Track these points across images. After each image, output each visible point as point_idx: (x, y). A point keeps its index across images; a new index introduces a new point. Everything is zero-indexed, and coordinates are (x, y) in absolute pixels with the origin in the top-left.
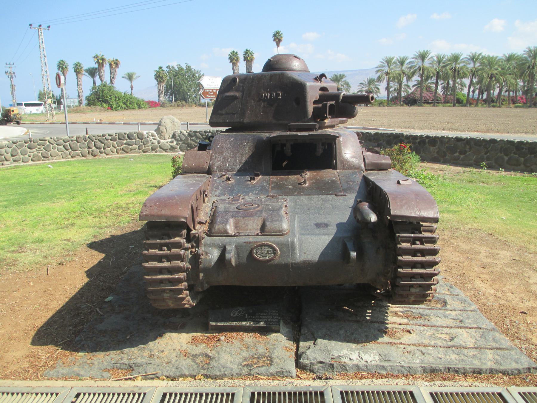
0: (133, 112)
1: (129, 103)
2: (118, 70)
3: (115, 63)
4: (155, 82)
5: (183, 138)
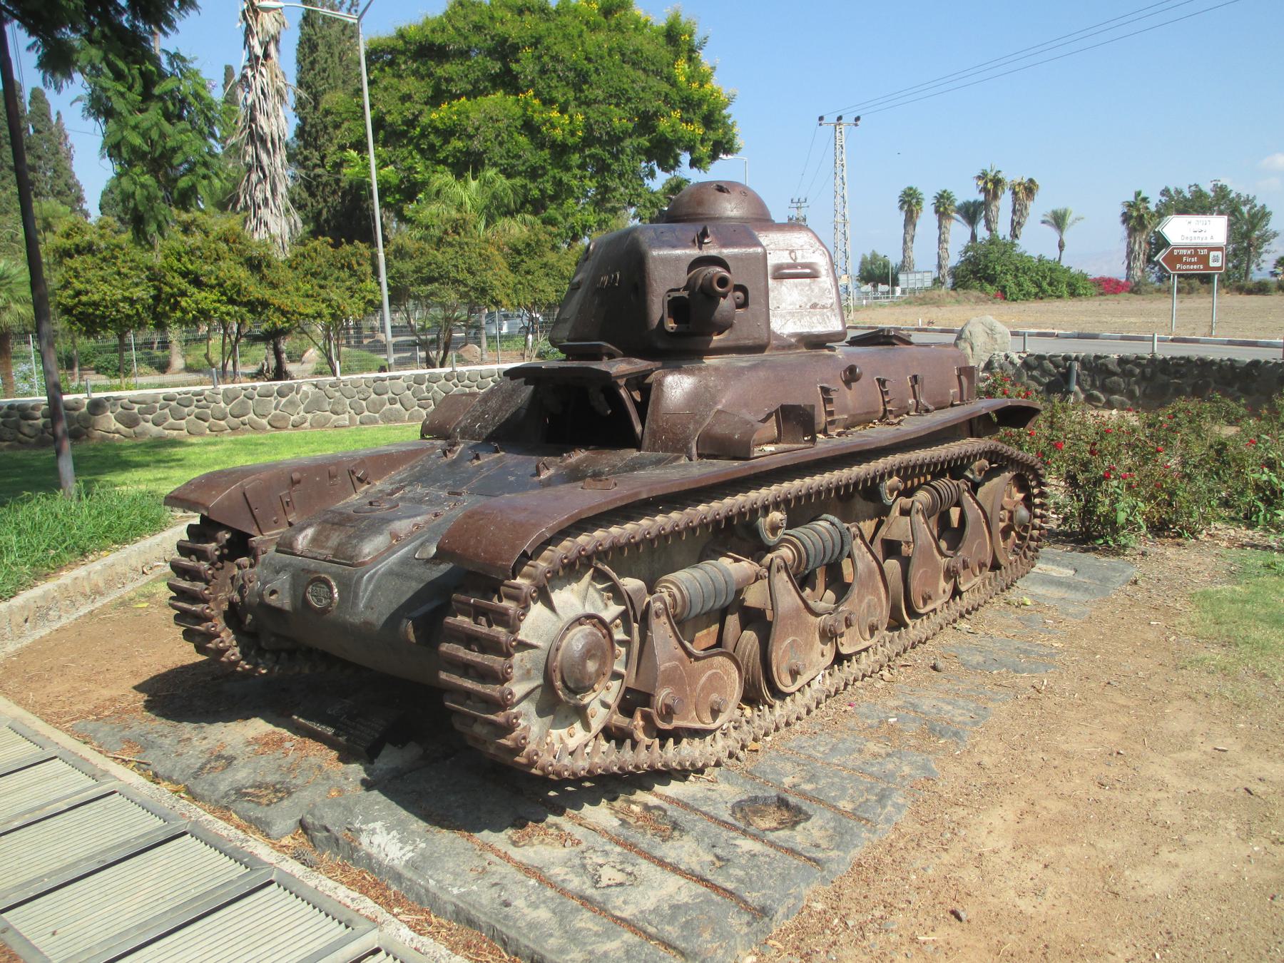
0: (1057, 304)
1: (1050, 282)
3: (1025, 188)
4: (1122, 231)
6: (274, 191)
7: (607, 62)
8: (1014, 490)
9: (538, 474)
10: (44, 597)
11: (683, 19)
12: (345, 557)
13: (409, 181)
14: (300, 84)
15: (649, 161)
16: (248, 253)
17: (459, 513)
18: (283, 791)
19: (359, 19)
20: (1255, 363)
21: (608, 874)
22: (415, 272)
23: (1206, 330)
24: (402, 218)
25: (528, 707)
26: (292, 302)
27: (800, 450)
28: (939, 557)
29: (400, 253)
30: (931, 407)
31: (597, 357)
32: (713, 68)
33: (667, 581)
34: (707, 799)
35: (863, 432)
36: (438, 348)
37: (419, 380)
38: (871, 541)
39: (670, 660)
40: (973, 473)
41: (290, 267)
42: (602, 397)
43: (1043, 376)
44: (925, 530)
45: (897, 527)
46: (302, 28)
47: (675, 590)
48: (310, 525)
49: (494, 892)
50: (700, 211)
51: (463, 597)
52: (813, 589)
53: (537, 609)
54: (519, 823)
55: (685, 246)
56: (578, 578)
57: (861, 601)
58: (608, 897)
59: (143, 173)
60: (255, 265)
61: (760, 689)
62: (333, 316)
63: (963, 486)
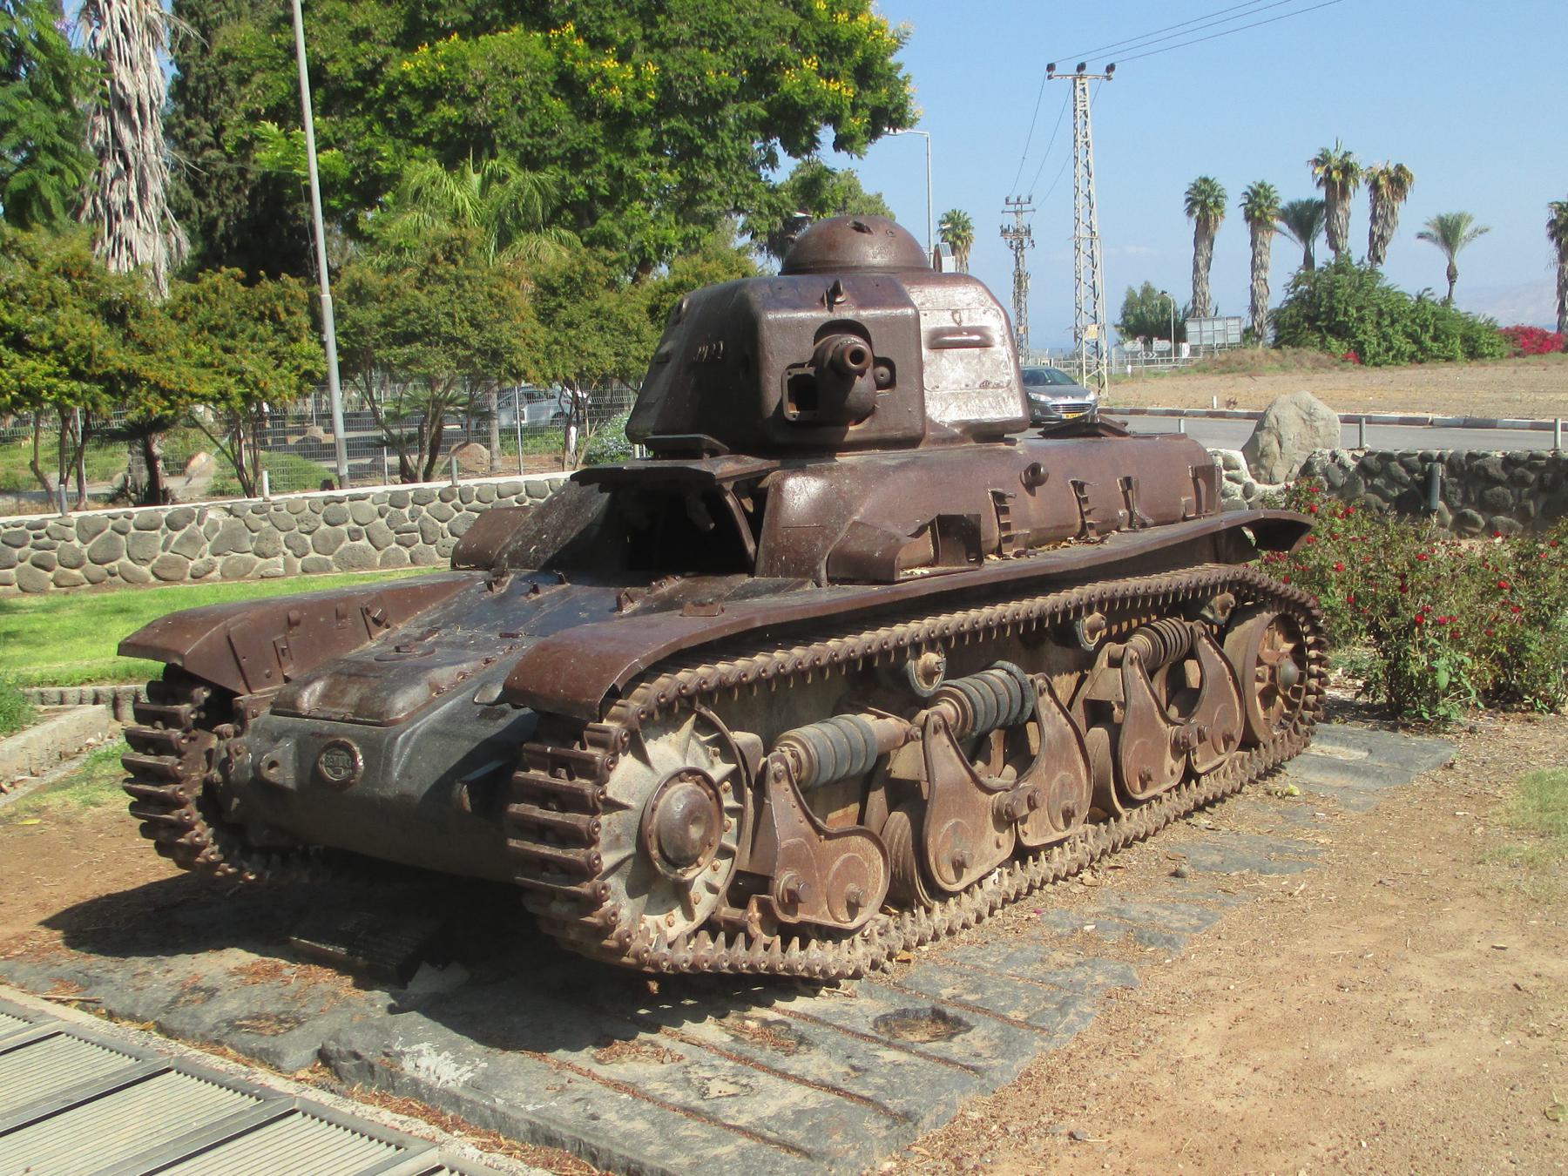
0: (1446, 371)
1: (1434, 335)
3: (1391, 181)
6: (142, 191)
8: (1279, 638)
9: (619, 608)
12: (372, 715)
13: (366, 172)
15: (766, 139)
16: (104, 296)
17: (517, 656)
18: (289, 1021)
21: (715, 1087)
22: (380, 325)
24: (352, 231)
25: (616, 883)
26: (179, 375)
27: (961, 574)
28: (1163, 725)
29: (358, 294)
30: (1149, 521)
31: (697, 455)
33: (788, 738)
34: (841, 1014)
35: (1052, 552)
36: (421, 450)
37: (397, 501)
39: (793, 835)
40: (1212, 610)
41: (174, 317)
42: (702, 506)
43: (1389, 486)
44: (1143, 692)
45: (1105, 683)
47: (799, 749)
49: (578, 1107)
50: (832, 257)
51: (537, 747)
52: (987, 762)
53: (627, 762)
54: (603, 1041)
55: (811, 307)
56: (677, 727)
57: (1051, 777)
58: (719, 1107)
60: (116, 314)
61: (910, 889)
63: (1199, 629)
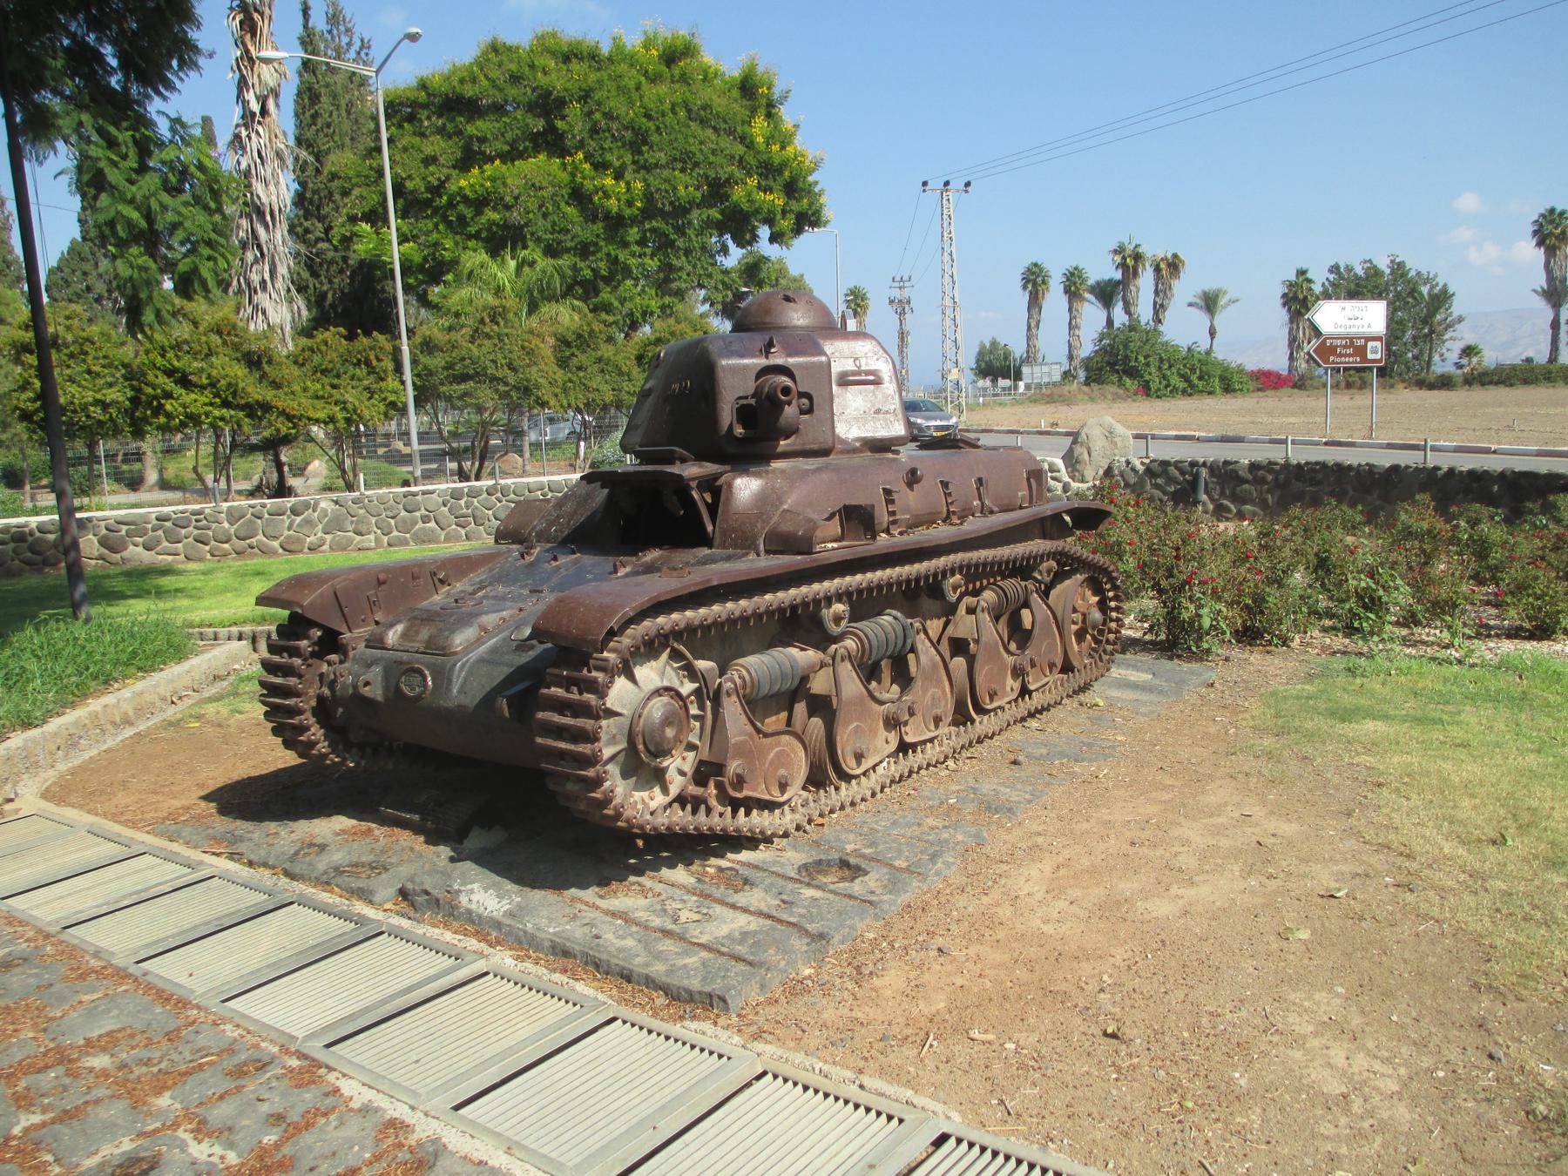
0: (1209, 402)
1: (1200, 376)
2: (1177, 285)
3: (1169, 265)
4: (1282, 315)
5: (1132, 480)
7: (669, 119)
8: (1088, 593)
9: (616, 572)
10: (75, 724)
11: (760, 69)
14: (299, 141)
15: (721, 235)
16: (246, 348)
17: (542, 606)
19: (377, 72)
20: (1395, 469)
21: (684, 915)
23: (1365, 432)
24: (424, 301)
27: (860, 547)
29: (428, 346)
31: (671, 462)
32: (796, 126)
34: (774, 863)
37: (456, 495)
38: (939, 641)
40: (1041, 573)
41: (296, 363)
42: (675, 498)
45: (963, 625)
46: (301, 75)
47: (744, 673)
48: (399, 622)
49: (586, 930)
51: (556, 671)
52: (879, 682)
53: (621, 683)
54: (604, 882)
55: (753, 356)
56: (656, 657)
57: (925, 692)
58: (687, 930)
59: (141, 255)
60: (254, 361)
62: (349, 421)
63: (1031, 587)
